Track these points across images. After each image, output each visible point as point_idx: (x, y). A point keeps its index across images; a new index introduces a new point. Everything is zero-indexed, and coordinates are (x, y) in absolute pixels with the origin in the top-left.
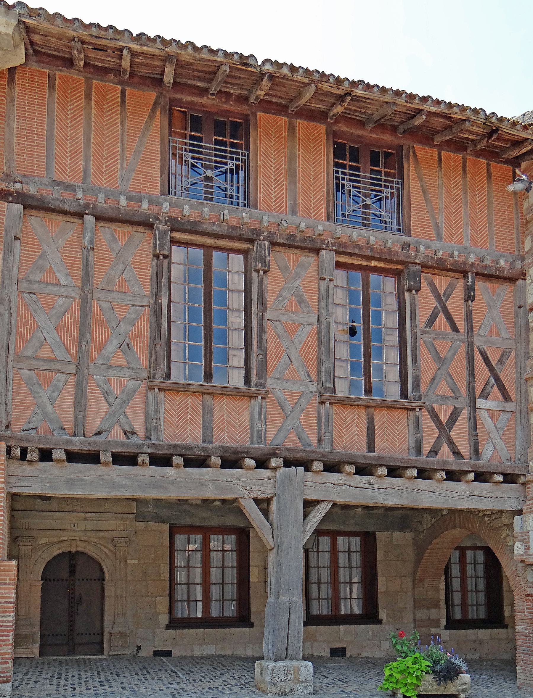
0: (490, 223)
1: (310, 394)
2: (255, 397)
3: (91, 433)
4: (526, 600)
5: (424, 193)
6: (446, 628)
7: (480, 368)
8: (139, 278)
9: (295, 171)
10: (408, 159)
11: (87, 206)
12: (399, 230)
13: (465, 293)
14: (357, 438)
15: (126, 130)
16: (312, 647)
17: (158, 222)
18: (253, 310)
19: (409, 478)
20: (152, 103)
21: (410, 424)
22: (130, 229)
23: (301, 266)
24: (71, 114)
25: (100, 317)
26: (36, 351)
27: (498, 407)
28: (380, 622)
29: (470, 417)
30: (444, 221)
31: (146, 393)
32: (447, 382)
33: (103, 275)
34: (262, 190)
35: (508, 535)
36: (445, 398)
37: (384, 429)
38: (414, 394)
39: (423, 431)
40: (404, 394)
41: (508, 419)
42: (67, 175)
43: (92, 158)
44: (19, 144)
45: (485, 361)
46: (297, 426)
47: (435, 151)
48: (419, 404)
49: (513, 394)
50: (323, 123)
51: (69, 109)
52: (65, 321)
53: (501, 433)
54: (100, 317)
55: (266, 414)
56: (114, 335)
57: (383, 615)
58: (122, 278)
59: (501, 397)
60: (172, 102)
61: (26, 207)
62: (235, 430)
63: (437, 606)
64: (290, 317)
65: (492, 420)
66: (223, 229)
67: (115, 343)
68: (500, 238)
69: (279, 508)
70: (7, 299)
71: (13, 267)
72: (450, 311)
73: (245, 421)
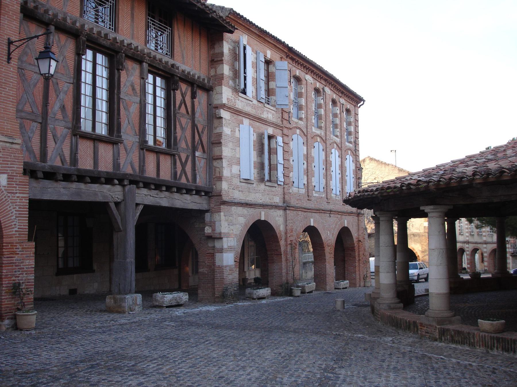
28: (94, 271)
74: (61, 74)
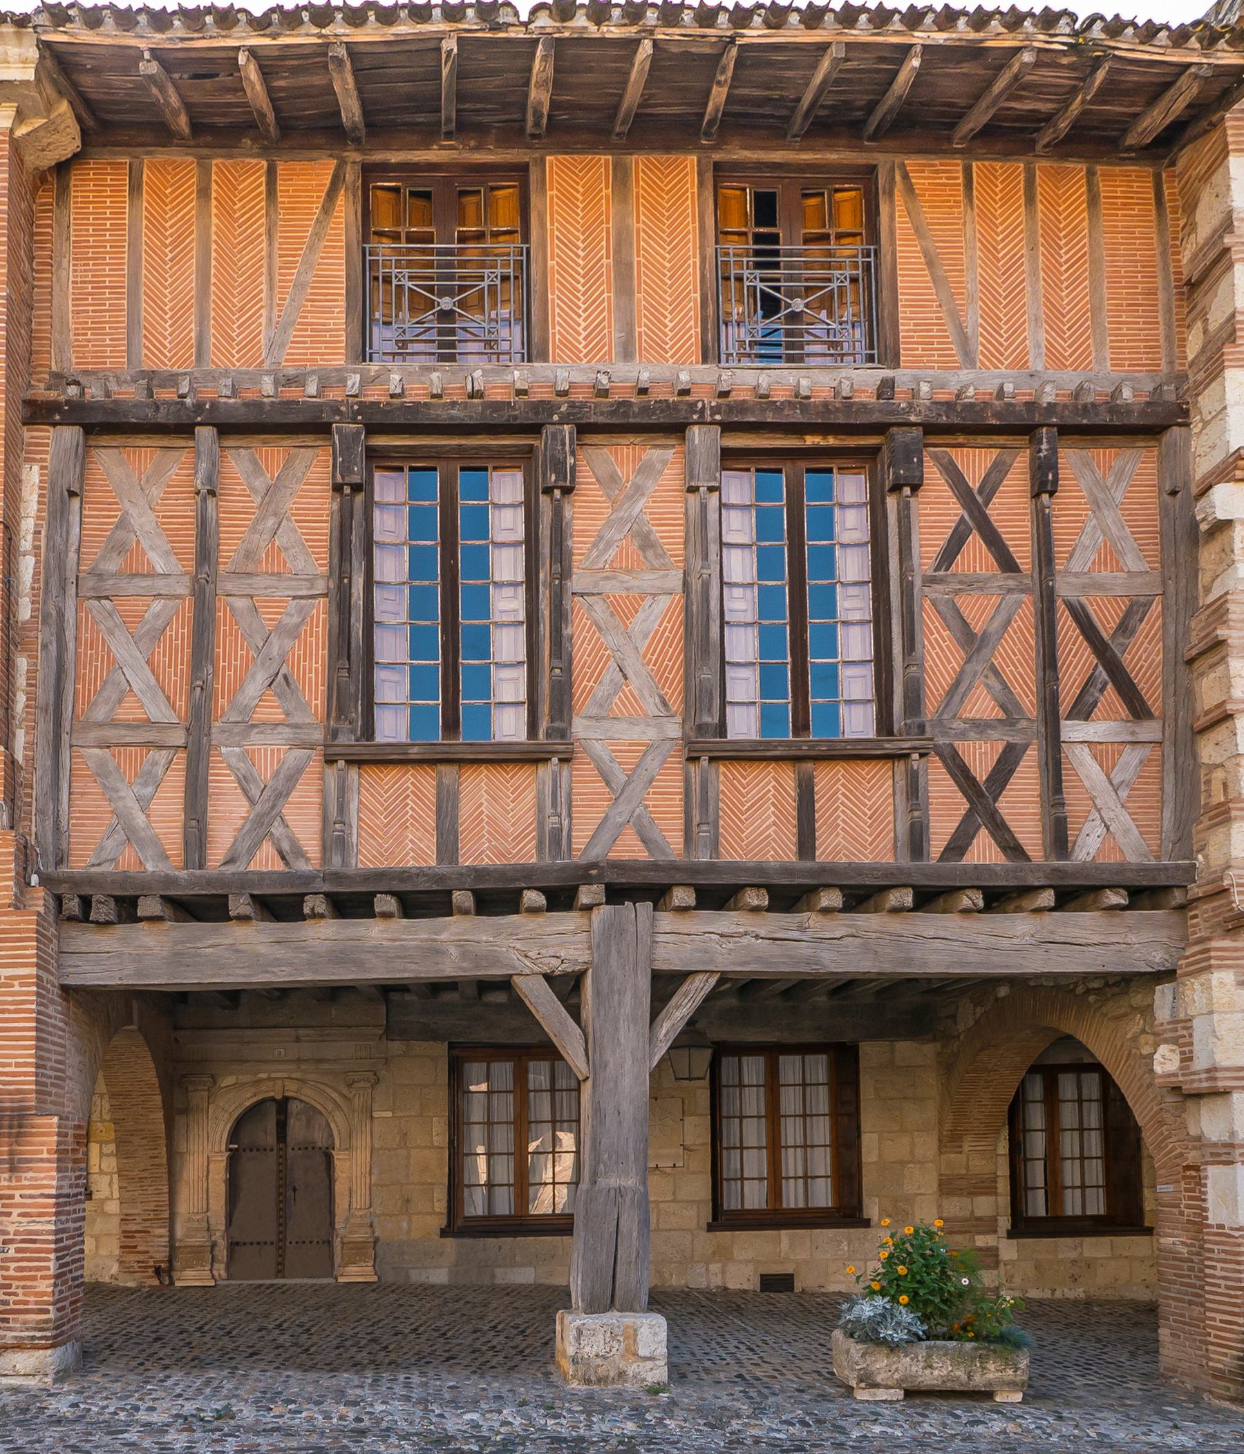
0: (1096, 310)
1: (668, 744)
2: (547, 760)
3: (216, 861)
4: (1184, 1177)
5: (930, 264)
6: (1011, 1235)
7: (1071, 650)
8: (307, 540)
9: (629, 266)
10: (891, 194)
11: (199, 407)
12: (871, 358)
13: (1032, 478)
14: (775, 832)
15: (276, 245)
16: (723, 1272)
17: (337, 418)
18: (541, 576)
19: (895, 911)
20: (328, 182)
21: (897, 791)
22: (289, 441)
23: (646, 470)
24: (171, 235)
25: (231, 629)
26: (112, 709)
27: (1117, 734)
28: (866, 1223)
29: (1047, 764)
30: (980, 321)
31: (322, 773)
32: (987, 686)
33: (235, 545)
34: (557, 318)
35: (1143, 1031)
36: (980, 727)
37: (838, 808)
38: (908, 721)
39: (928, 804)
40: (885, 724)
41: (1141, 762)
42: (165, 356)
43: (213, 314)
44: (78, 312)
45: (1083, 632)
46: (639, 816)
47: (957, 165)
48: (917, 743)
49: (1156, 700)
50: (689, 152)
51: (167, 225)
52: (165, 645)
53: (1124, 794)
54: (231, 629)
55: (569, 795)
56: (259, 661)
57: (872, 1209)
58: (273, 545)
59: (1123, 711)
60: (369, 171)
61: (90, 430)
62: (506, 833)
63: (991, 1190)
64: (622, 582)
65: (1102, 768)
66: (474, 413)
67: (261, 678)
68: (1122, 341)
69: (597, 993)
70: (54, 613)
71: (67, 551)
72: (996, 524)
73: (526, 813)
74: (273, 574)
